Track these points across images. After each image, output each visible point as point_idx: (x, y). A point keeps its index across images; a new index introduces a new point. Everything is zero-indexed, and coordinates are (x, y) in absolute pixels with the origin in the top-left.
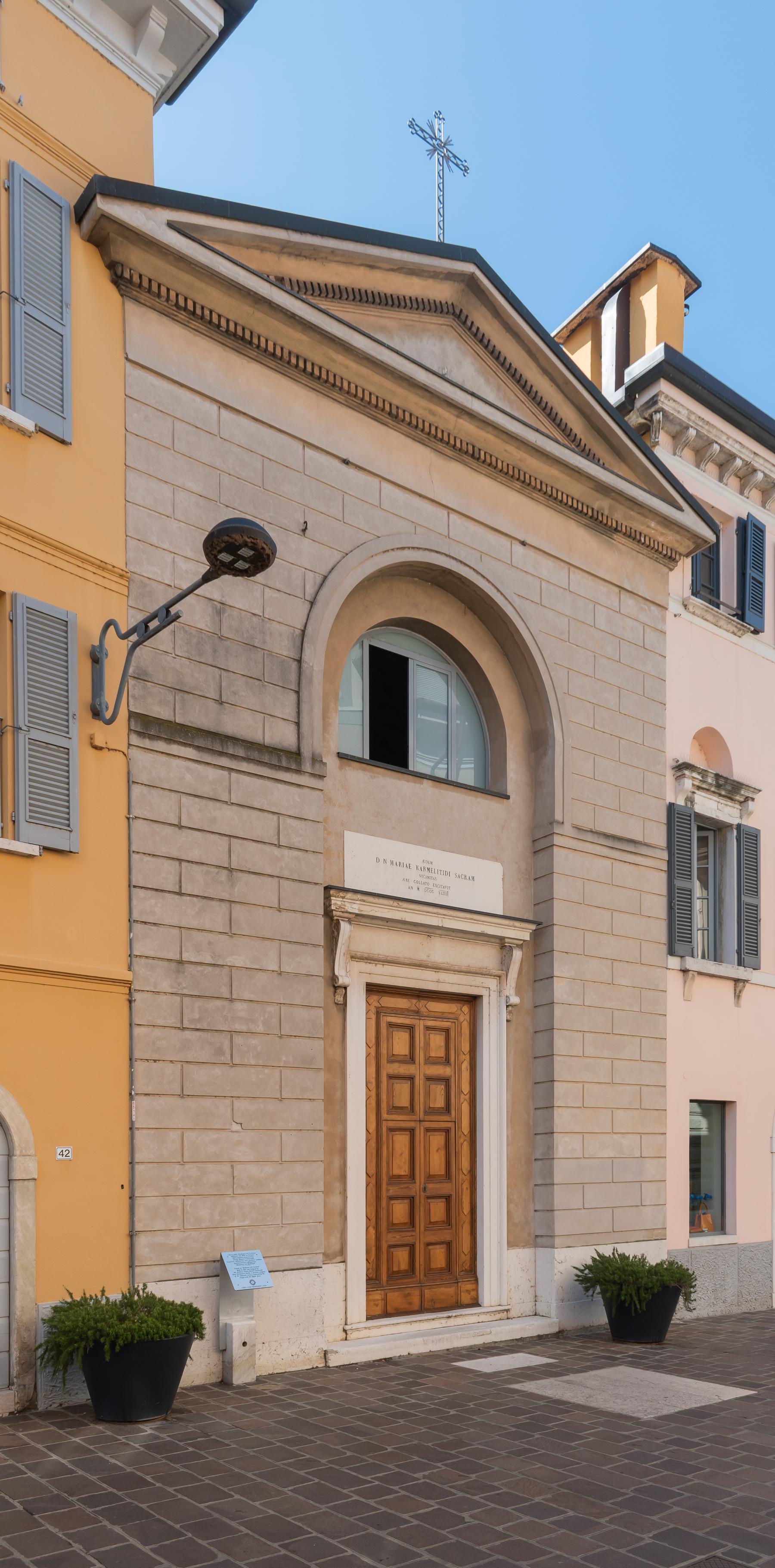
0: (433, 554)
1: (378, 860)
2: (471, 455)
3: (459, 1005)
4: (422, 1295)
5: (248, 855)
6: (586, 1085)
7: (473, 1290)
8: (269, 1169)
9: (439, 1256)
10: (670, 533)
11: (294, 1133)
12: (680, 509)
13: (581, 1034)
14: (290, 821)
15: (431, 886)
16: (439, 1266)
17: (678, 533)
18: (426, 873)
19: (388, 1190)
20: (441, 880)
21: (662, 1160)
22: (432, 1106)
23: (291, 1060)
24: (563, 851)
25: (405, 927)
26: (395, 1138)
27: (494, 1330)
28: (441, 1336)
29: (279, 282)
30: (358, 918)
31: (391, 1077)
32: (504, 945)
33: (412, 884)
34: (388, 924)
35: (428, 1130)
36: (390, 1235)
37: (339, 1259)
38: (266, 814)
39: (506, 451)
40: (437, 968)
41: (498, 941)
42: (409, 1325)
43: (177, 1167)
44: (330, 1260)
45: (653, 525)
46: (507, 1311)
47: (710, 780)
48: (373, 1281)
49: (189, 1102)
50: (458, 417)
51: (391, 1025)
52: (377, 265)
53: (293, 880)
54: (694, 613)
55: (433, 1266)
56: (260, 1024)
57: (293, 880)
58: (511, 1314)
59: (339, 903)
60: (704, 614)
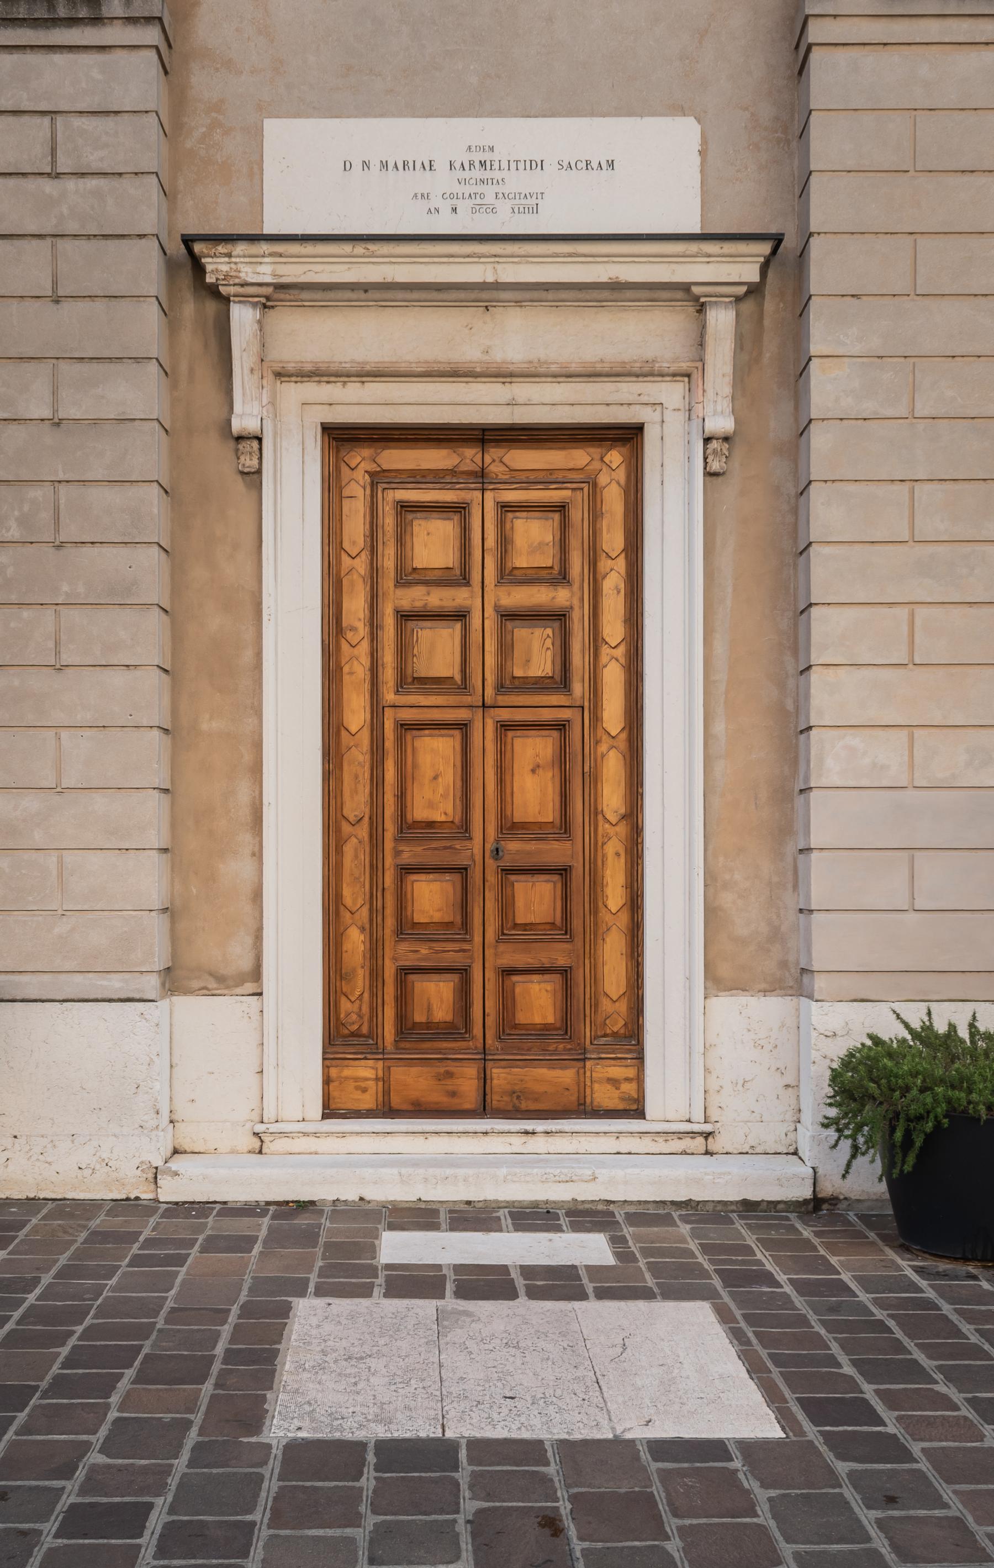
1: (347, 166)
3: (595, 451)
4: (484, 1079)
6: (921, 612)
7: (628, 1080)
9: (538, 1001)
11: (88, 733)
13: (906, 487)
14: (77, 122)
15: (490, 199)
16: (538, 1020)
18: (478, 173)
19: (397, 853)
20: (517, 182)
22: (518, 673)
23: (81, 589)
24: (841, 55)
25: (415, 295)
26: (418, 743)
27: (603, 1174)
28: (449, 1172)
30: (274, 297)
31: (404, 617)
32: (692, 299)
33: (436, 202)
34: (370, 295)
35: (505, 727)
36: (404, 947)
37: (250, 987)
38: (25, 119)
40: (504, 375)
41: (680, 295)
42: (420, 1140)
44: (228, 987)
46: (707, 1135)
48: (340, 1039)
51: (405, 508)
53: (89, 237)
55: (521, 1018)
56: (13, 524)
57: (89, 237)
58: (713, 1145)
59: (225, 268)
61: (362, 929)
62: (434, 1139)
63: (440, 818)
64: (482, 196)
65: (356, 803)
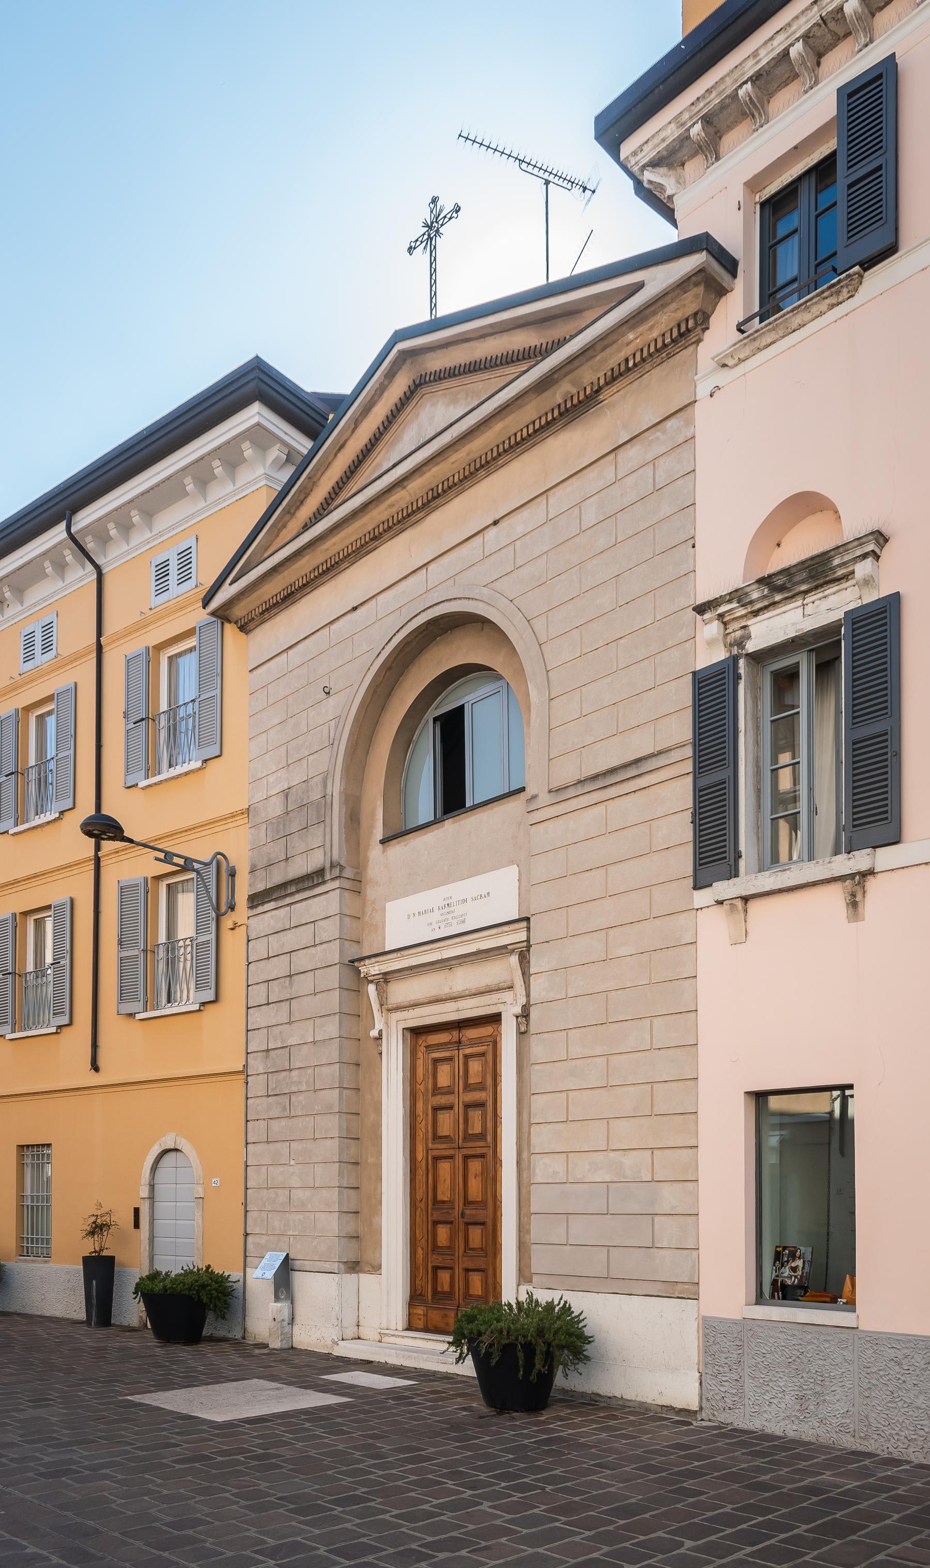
0: (452, 603)
2: (434, 499)
5: (302, 961)
6: (571, 1094)
8: (308, 1193)
10: (658, 317)
12: (640, 286)
15: (450, 921)
17: (664, 306)
18: (448, 909)
19: (432, 1215)
20: (459, 910)
21: (690, 1185)
29: (306, 527)
30: (386, 977)
36: (434, 1256)
39: (453, 463)
42: (425, 1342)
43: (265, 1191)
45: (631, 336)
47: (755, 595)
48: (415, 1298)
49: (271, 1146)
50: (404, 488)
52: (341, 442)
54: (741, 361)
60: (756, 344)
61: (422, 1249)
62: (430, 1342)
63: (446, 1199)
64: (447, 919)
65: (420, 1193)
